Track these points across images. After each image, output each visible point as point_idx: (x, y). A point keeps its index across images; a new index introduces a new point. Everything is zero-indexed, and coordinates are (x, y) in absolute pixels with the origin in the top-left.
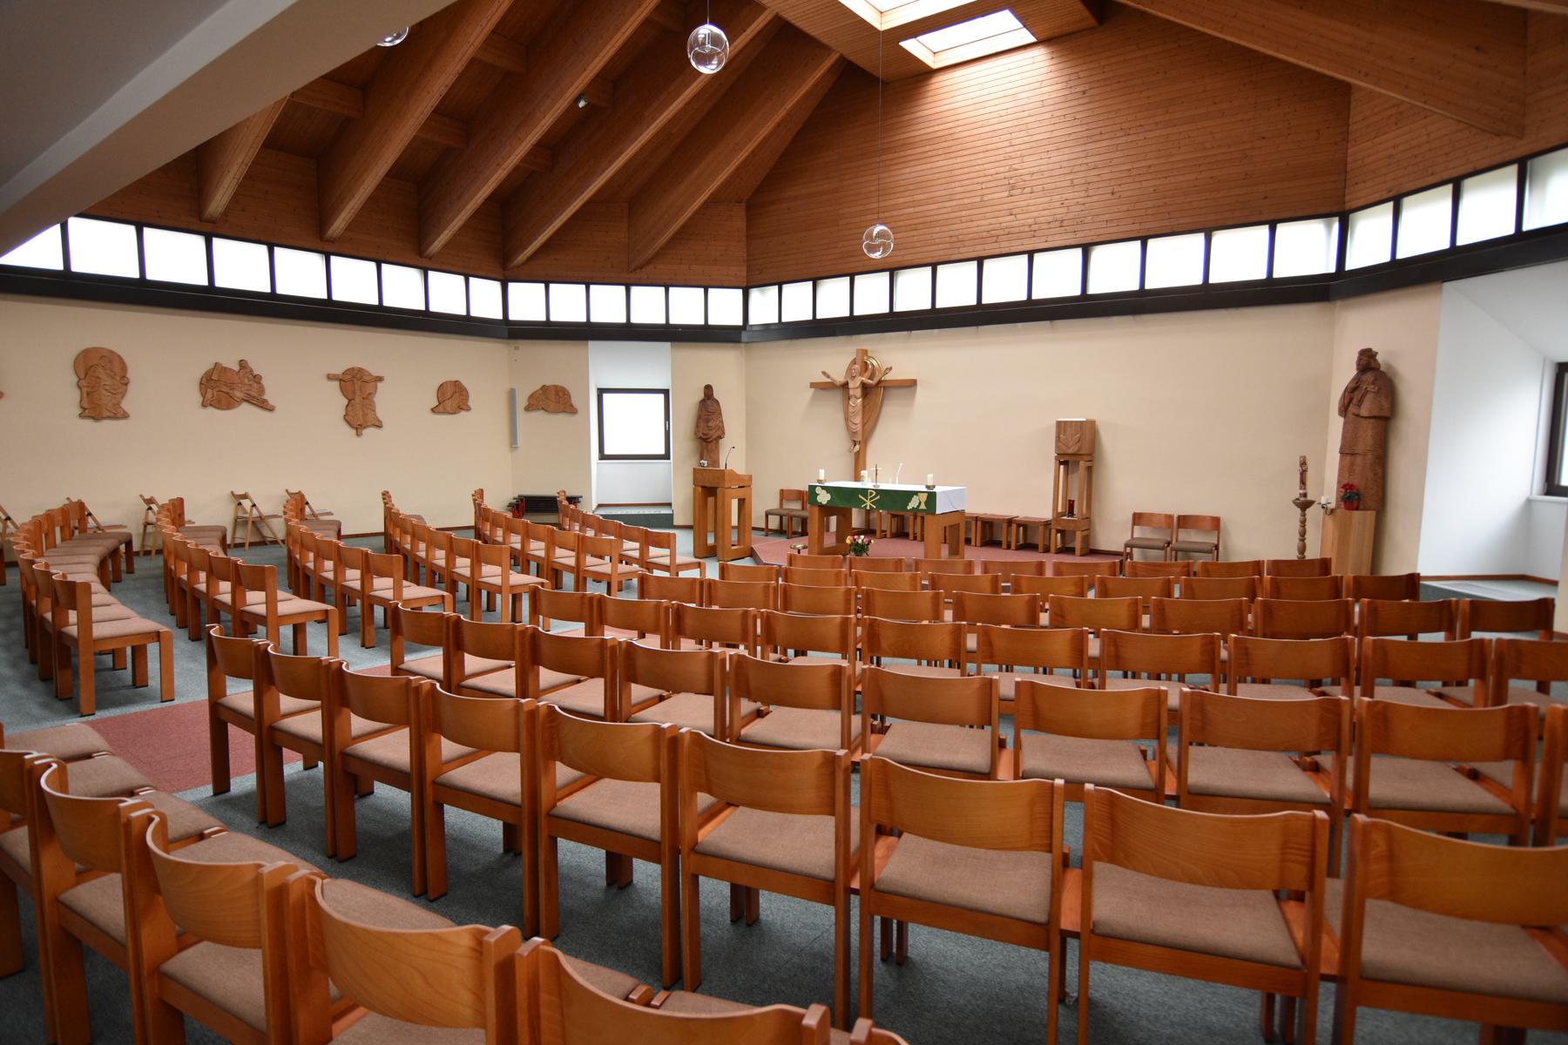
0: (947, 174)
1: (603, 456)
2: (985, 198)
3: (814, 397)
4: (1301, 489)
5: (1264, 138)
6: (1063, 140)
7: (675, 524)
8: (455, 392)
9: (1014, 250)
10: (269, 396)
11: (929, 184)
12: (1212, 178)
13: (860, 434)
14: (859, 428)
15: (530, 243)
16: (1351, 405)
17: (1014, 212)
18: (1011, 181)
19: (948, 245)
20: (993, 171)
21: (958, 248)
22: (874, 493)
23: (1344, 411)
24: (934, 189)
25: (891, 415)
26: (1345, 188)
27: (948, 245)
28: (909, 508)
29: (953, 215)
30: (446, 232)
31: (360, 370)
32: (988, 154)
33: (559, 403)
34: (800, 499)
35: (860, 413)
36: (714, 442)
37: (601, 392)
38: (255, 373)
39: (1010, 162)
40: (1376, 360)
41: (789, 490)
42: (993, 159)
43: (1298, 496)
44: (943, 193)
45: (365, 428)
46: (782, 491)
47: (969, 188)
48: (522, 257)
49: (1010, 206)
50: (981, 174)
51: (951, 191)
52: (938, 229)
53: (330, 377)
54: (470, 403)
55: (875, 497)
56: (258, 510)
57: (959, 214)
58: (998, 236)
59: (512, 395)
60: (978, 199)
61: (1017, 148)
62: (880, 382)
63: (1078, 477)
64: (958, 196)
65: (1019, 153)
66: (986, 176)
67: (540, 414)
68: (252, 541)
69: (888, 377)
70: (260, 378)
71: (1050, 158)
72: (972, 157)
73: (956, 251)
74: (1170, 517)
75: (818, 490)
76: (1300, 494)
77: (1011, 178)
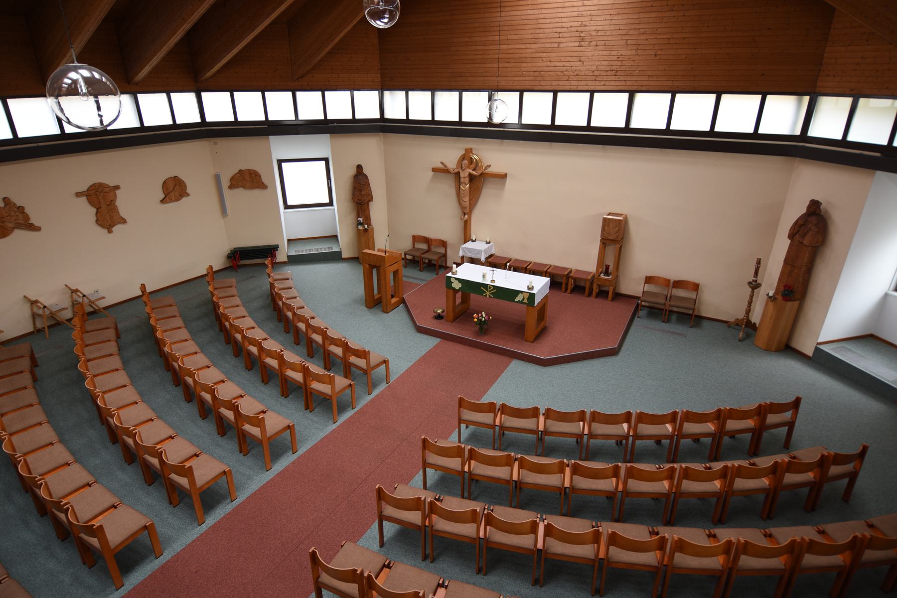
0: (533, 21)
1: (287, 207)
2: (561, 45)
3: (434, 177)
4: (754, 277)
5: (769, 29)
6: (623, 7)
7: (343, 257)
8: (175, 185)
9: (580, 88)
10: (33, 220)
11: (520, 27)
12: (728, 54)
13: (468, 208)
14: (467, 204)
15: (215, 65)
16: (798, 234)
17: (583, 59)
18: (582, 35)
19: (532, 78)
20: (569, 24)
21: (540, 81)
22: (492, 288)
23: (791, 236)
24: (523, 32)
25: (488, 192)
26: (820, 70)
27: (532, 78)
28: (516, 300)
29: (537, 55)
30: (147, 67)
31: (101, 185)
32: (566, 10)
33: (253, 182)
34: (426, 243)
35: (468, 194)
36: (366, 204)
37: (280, 162)
38: (18, 205)
39: (582, 19)
40: (820, 209)
41: (417, 236)
42: (569, 14)
43: (751, 281)
44: (530, 36)
45: (113, 226)
46: (414, 237)
47: (550, 36)
48: (209, 74)
49: (580, 54)
50: (560, 25)
51: (536, 36)
52: (525, 64)
53: (78, 195)
54: (188, 191)
55: (492, 290)
56: (48, 309)
57: (541, 55)
58: (569, 76)
59: (217, 179)
60: (556, 45)
61: (587, 8)
62: (482, 174)
63: (611, 251)
64: (541, 41)
65: (589, 13)
66: (563, 27)
67: (240, 191)
68: (49, 324)
69: (489, 170)
70: (23, 208)
71: (612, 20)
72: (555, 11)
73: (538, 83)
74: (669, 281)
75: (452, 280)
76: (753, 280)
77: (582, 32)
